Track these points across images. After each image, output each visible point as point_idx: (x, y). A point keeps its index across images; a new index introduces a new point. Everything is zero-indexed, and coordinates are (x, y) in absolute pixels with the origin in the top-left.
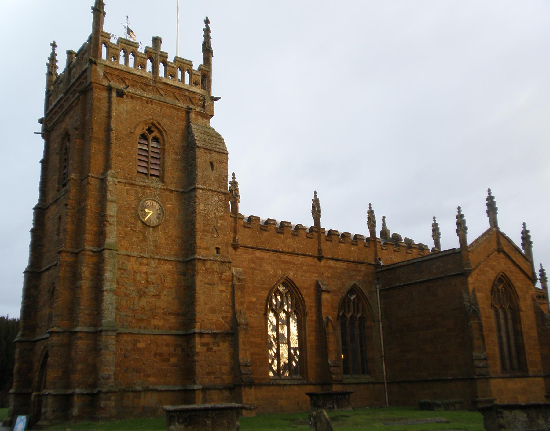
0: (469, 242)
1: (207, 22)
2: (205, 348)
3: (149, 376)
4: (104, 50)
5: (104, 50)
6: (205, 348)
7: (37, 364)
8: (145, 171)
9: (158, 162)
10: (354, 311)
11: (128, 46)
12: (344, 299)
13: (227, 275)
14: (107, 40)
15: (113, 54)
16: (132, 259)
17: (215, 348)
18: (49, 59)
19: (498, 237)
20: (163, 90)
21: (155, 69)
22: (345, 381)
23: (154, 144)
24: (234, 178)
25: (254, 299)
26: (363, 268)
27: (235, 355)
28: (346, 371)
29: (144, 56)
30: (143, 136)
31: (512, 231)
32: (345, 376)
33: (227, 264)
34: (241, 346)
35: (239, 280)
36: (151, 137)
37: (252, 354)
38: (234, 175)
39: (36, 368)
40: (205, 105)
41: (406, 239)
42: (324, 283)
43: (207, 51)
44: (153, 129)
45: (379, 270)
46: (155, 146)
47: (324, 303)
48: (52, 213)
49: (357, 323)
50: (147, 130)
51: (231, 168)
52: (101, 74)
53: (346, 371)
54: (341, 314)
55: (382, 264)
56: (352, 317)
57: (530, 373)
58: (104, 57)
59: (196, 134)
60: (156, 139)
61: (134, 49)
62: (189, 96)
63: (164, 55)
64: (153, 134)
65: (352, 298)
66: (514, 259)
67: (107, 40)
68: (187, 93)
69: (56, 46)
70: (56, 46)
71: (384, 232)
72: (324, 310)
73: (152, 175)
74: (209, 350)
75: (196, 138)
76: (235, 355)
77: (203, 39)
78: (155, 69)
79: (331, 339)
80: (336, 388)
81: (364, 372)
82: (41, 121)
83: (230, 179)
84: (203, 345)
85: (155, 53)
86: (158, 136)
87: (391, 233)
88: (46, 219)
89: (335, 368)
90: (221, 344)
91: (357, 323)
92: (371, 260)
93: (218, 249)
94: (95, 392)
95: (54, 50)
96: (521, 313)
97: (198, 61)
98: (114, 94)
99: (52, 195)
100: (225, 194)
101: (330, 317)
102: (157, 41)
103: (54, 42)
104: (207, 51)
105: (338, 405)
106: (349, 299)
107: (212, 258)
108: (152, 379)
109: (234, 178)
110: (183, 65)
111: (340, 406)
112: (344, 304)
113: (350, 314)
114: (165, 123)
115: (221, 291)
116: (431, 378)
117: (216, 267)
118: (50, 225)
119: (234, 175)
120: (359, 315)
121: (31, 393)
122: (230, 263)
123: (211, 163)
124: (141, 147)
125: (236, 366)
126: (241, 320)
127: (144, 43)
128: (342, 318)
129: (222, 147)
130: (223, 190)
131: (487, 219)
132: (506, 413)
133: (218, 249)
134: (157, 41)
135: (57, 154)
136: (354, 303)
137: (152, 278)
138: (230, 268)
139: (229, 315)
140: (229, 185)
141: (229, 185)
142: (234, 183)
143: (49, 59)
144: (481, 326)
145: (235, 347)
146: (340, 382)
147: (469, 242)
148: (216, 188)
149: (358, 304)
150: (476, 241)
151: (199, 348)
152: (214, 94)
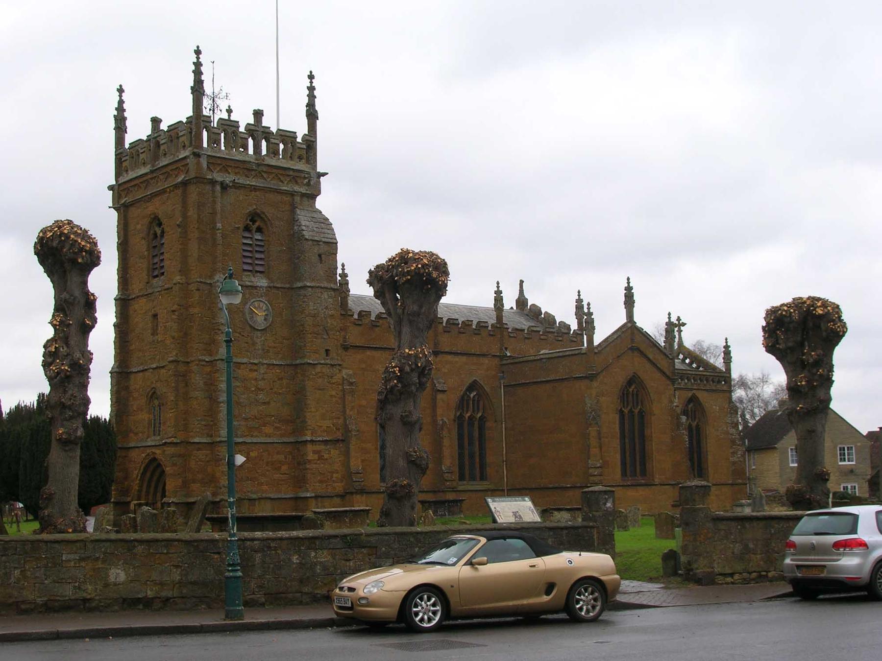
0: (596, 343)
1: (311, 77)
2: (316, 456)
3: (262, 484)
4: (205, 134)
5: (205, 134)
6: (316, 456)
7: (136, 472)
8: (250, 268)
9: (262, 256)
10: (473, 411)
11: (229, 126)
12: (463, 397)
13: (337, 378)
14: (208, 124)
15: (214, 140)
16: (242, 366)
17: (326, 456)
18: (116, 109)
19: (633, 333)
20: (265, 172)
21: (257, 147)
22: (460, 488)
23: (258, 236)
24: (343, 269)
25: (364, 403)
26: (486, 361)
27: (346, 464)
28: (462, 478)
29: (246, 136)
30: (247, 229)
31: (651, 323)
32: (460, 483)
33: (338, 367)
34: (352, 453)
35: (351, 384)
36: (255, 227)
37: (363, 461)
38: (343, 265)
39: (135, 476)
40: (309, 184)
41: (546, 313)
42: (441, 380)
43: (312, 115)
44: (256, 218)
45: (505, 362)
46: (259, 238)
47: (440, 403)
48: (140, 307)
49: (476, 423)
50: (251, 221)
51: (341, 258)
52: (205, 165)
53: (462, 478)
54: (458, 414)
55: (508, 354)
56: (471, 418)
57: (657, 481)
58: (205, 145)
59: (303, 223)
60: (259, 230)
61: (234, 129)
62: (296, 176)
63: (267, 130)
64: (257, 224)
65: (472, 395)
66: (651, 356)
67: (208, 124)
68: (291, 173)
69: (123, 91)
70: (123, 91)
71: (521, 302)
72: (439, 411)
73: (257, 272)
74: (321, 458)
75: (304, 228)
76: (346, 464)
77: (306, 100)
78: (257, 147)
79: (446, 442)
80: (451, 496)
81: (483, 478)
82: (111, 188)
83: (339, 271)
84: (314, 452)
85: (257, 130)
86: (262, 225)
87: (529, 304)
88: (131, 312)
89: (449, 475)
90: (332, 451)
91: (476, 423)
92: (495, 350)
93: (327, 351)
94: (218, 500)
95: (120, 96)
96: (653, 418)
97: (301, 129)
98: (218, 188)
99: (136, 287)
100: (334, 290)
101: (445, 419)
102: (258, 114)
103: (121, 86)
104: (312, 115)
105: (449, 512)
106: (469, 396)
107: (323, 362)
108: (265, 487)
109: (343, 269)
110: (287, 137)
111: (452, 513)
112: (463, 403)
113: (469, 414)
114: (269, 212)
115: (331, 396)
116: (551, 486)
117: (327, 370)
118: (140, 321)
119: (343, 265)
120: (480, 415)
121: (129, 502)
122: (340, 365)
123: (320, 256)
124: (245, 241)
125: (349, 475)
126: (352, 427)
127: (244, 119)
128: (460, 419)
129: (330, 236)
130: (332, 286)
131: (623, 312)
132: (556, 513)
133: (327, 351)
134: (258, 114)
135: (144, 238)
136: (473, 401)
137: (261, 384)
138: (340, 370)
139: (341, 421)
140: (339, 278)
141: (339, 278)
142: (344, 275)
143: (116, 109)
144: (599, 433)
145: (347, 454)
146: (454, 490)
147: (596, 343)
148: (325, 284)
149: (478, 401)
150: (600, 344)
151: (311, 456)
152: (320, 169)
